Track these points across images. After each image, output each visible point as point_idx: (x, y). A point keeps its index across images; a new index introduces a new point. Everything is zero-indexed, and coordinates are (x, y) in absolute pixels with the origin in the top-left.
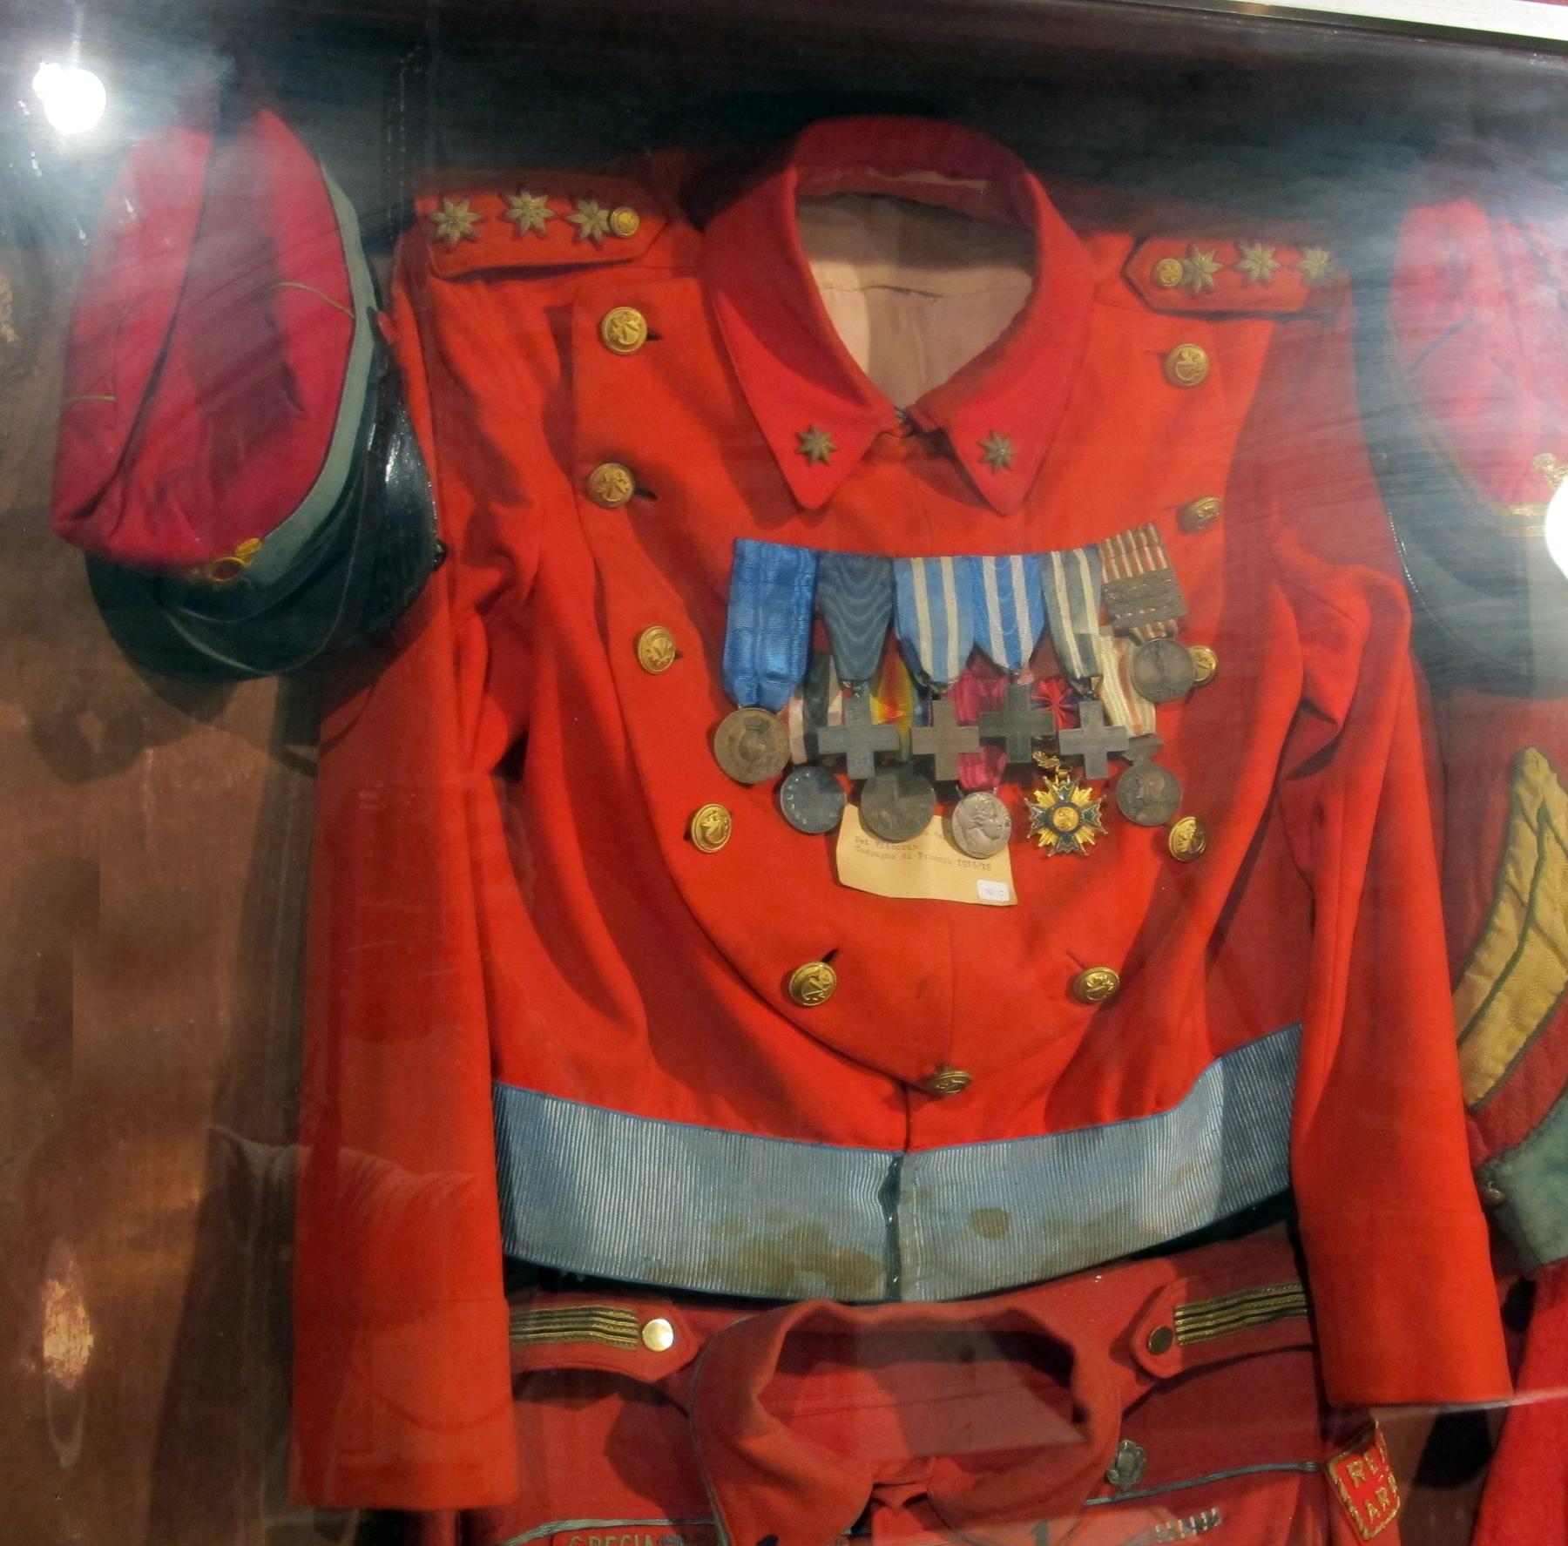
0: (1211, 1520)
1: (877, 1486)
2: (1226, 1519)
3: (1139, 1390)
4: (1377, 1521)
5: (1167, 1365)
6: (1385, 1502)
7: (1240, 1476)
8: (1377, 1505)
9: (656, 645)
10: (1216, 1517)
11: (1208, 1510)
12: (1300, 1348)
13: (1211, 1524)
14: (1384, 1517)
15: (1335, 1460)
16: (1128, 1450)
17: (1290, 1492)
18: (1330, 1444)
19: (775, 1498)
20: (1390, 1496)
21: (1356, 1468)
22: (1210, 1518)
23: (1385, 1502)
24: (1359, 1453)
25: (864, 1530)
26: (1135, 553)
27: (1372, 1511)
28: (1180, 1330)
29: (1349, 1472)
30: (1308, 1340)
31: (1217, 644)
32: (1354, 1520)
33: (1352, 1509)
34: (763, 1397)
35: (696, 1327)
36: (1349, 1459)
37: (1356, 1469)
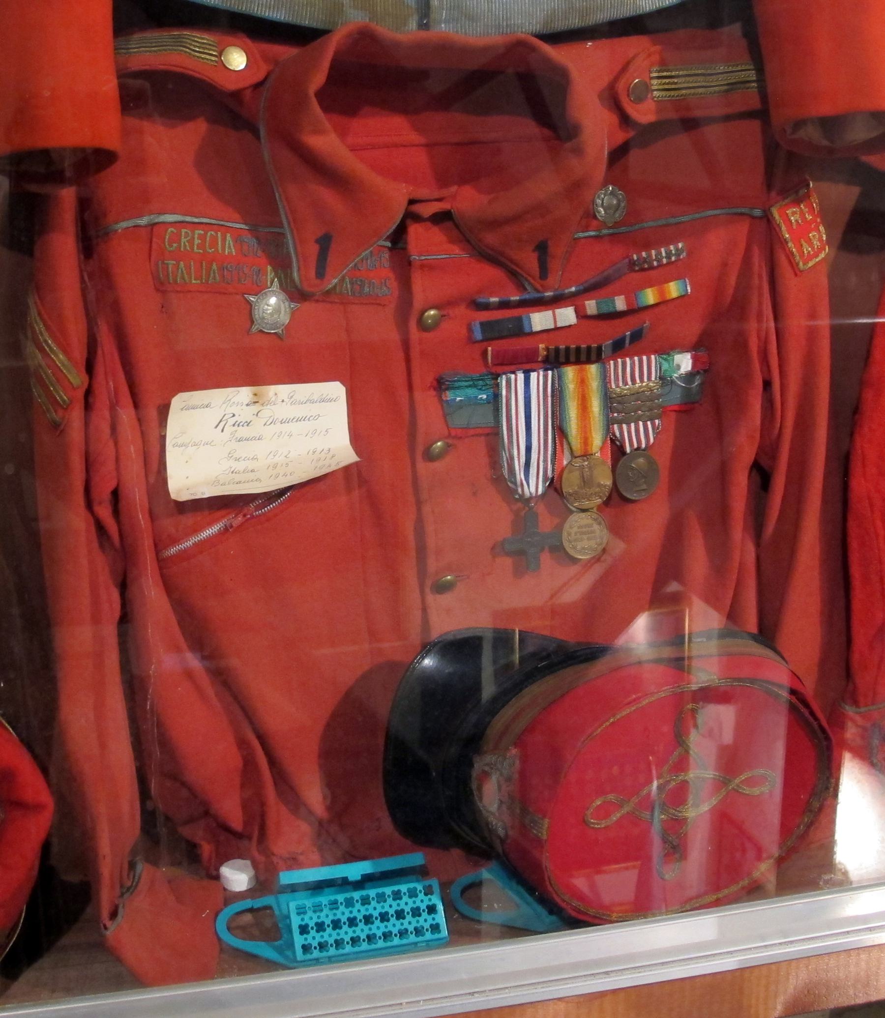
0: (678, 252)
1: (412, 202)
2: (690, 254)
3: (621, 137)
4: (810, 257)
5: (644, 114)
6: (816, 243)
7: (702, 218)
8: (811, 244)
9: (237, 60)
10: (682, 250)
11: (675, 243)
12: (750, 115)
13: (678, 255)
14: (816, 256)
15: (778, 205)
16: (612, 193)
17: (742, 230)
18: (773, 194)
19: (327, 195)
20: (820, 240)
21: (794, 213)
22: (677, 249)
23: (816, 243)
24: (797, 202)
25: (400, 245)
26: (529, 278)
27: (807, 249)
28: (653, 88)
29: (791, 217)
30: (755, 103)
31: (694, 348)
32: (792, 253)
33: (790, 244)
34: (320, 95)
35: (266, 59)
36: (788, 206)
37: (794, 214)
